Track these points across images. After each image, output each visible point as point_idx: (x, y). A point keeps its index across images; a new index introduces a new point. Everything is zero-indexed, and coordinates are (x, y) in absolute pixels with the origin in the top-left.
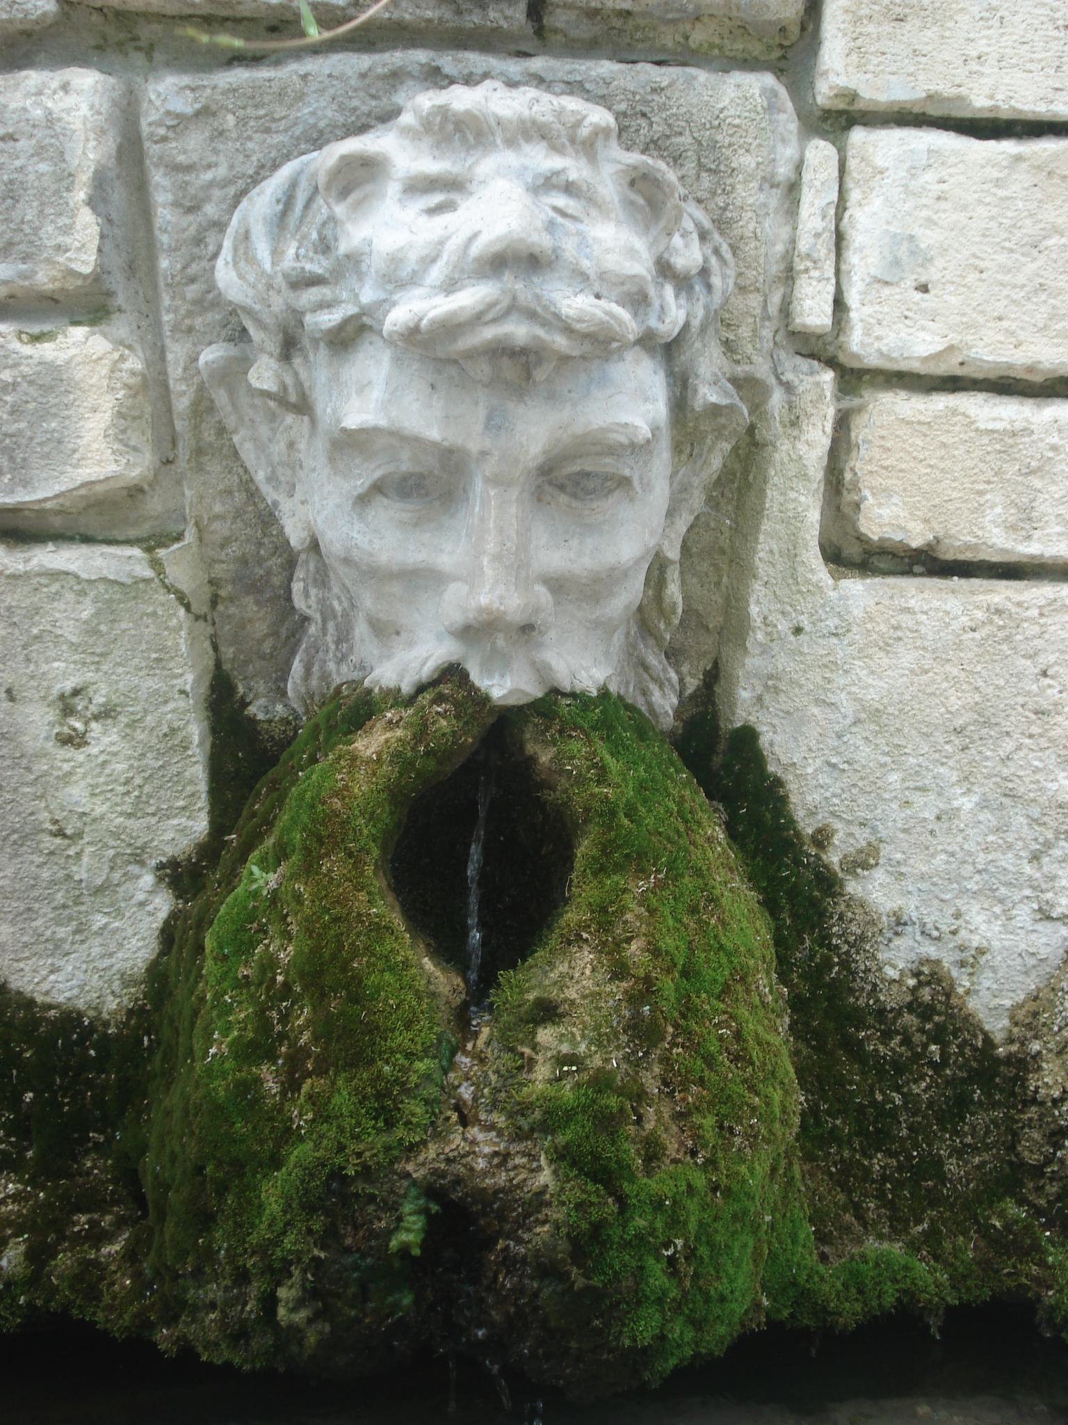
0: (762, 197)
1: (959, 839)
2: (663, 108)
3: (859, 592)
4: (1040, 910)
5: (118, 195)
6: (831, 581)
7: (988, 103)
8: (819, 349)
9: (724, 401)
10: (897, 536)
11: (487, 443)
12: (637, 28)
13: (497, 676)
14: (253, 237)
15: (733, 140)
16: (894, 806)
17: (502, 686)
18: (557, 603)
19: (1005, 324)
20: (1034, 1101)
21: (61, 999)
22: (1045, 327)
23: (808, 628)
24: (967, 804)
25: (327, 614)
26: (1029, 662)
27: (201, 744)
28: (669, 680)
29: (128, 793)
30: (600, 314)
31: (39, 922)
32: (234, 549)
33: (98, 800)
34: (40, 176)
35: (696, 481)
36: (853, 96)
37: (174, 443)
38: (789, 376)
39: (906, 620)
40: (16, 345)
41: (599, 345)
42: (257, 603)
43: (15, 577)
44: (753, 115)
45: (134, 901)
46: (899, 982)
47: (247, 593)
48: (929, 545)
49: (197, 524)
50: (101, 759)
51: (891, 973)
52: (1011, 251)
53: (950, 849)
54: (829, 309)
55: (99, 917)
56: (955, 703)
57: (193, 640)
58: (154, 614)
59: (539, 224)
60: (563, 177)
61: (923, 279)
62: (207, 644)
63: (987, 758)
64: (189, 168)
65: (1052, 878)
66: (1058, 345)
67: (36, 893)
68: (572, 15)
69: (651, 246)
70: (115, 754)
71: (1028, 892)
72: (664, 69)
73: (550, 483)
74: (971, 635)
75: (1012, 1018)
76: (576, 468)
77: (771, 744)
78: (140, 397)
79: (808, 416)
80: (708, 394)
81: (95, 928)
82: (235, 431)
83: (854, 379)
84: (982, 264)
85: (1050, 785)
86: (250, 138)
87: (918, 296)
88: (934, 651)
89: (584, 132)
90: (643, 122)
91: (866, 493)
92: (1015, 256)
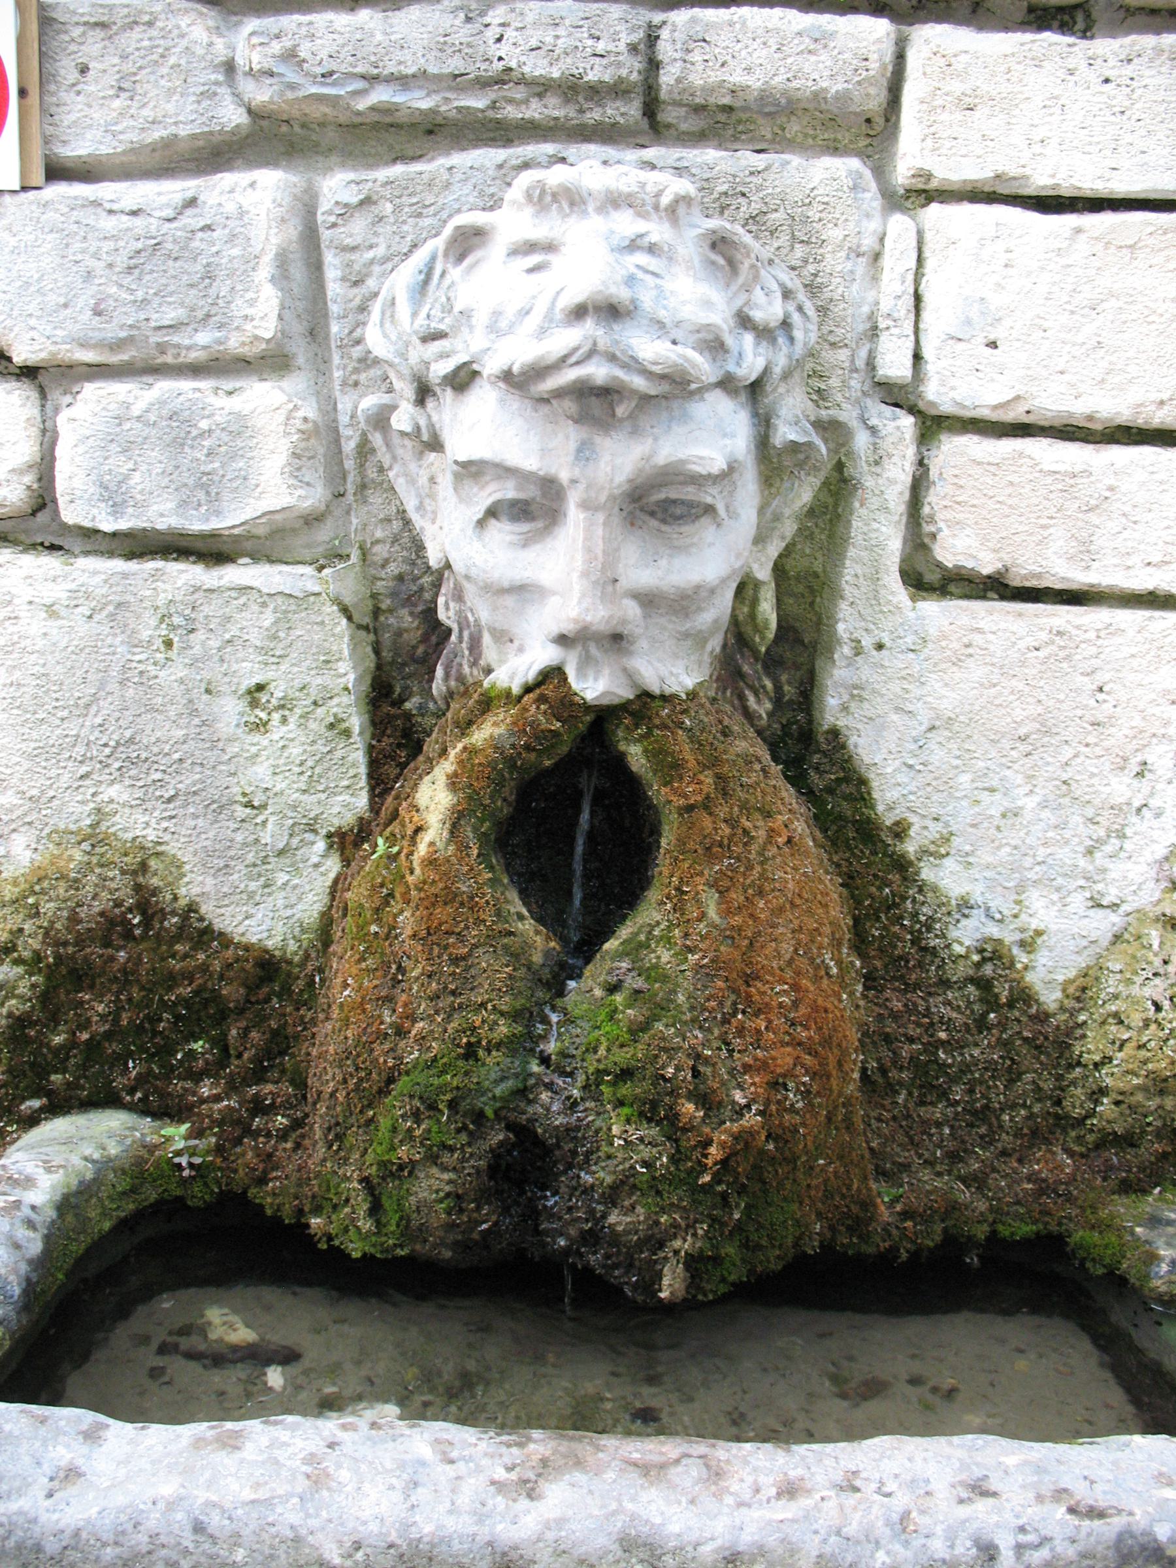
0: (849, 265)
1: (1022, 834)
2: (759, 188)
3: (936, 613)
4: (1092, 898)
5: (298, 272)
6: (909, 603)
7: (1050, 182)
8: (898, 396)
9: (801, 439)
10: (970, 564)
11: (577, 472)
12: (739, 122)
13: (591, 679)
14: (398, 302)
15: (823, 215)
16: (964, 803)
17: (593, 686)
18: (646, 616)
19: (1066, 377)
20: (1079, 1064)
21: (254, 940)
22: (1103, 381)
23: (888, 645)
24: (1030, 803)
25: (463, 624)
26: (1086, 679)
27: (361, 734)
28: (764, 687)
29: (302, 773)
30: (673, 357)
31: (236, 876)
32: (393, 569)
33: (279, 778)
34: (232, 259)
35: (787, 512)
36: (929, 176)
37: (344, 478)
38: (873, 421)
39: (978, 639)
40: (212, 399)
41: (676, 388)
42: (411, 614)
43: (211, 591)
44: (840, 194)
45: (309, 863)
46: (966, 957)
47: (403, 606)
48: (999, 573)
49: (361, 548)
50: (281, 744)
51: (958, 949)
52: (1072, 312)
53: (1013, 842)
54: (908, 361)
55: (282, 874)
56: (1019, 714)
57: (355, 645)
58: (322, 623)
59: (619, 278)
60: (647, 240)
61: (992, 337)
62: (369, 649)
63: (1048, 764)
64: (354, 249)
65: (1104, 871)
66: (1114, 397)
67: (232, 853)
68: (682, 111)
69: (730, 301)
70: (292, 740)
71: (1082, 882)
72: (762, 156)
73: (642, 510)
74: (1036, 653)
75: (1064, 991)
76: (662, 496)
77: (856, 746)
78: (312, 441)
79: (890, 456)
80: (785, 433)
81: (279, 883)
82: (390, 468)
83: (933, 426)
84: (1046, 325)
85: (1102, 789)
86: (404, 222)
87: (989, 350)
88: (1001, 667)
89: (665, 200)
90: (741, 200)
91: (941, 525)
92: (1075, 317)
